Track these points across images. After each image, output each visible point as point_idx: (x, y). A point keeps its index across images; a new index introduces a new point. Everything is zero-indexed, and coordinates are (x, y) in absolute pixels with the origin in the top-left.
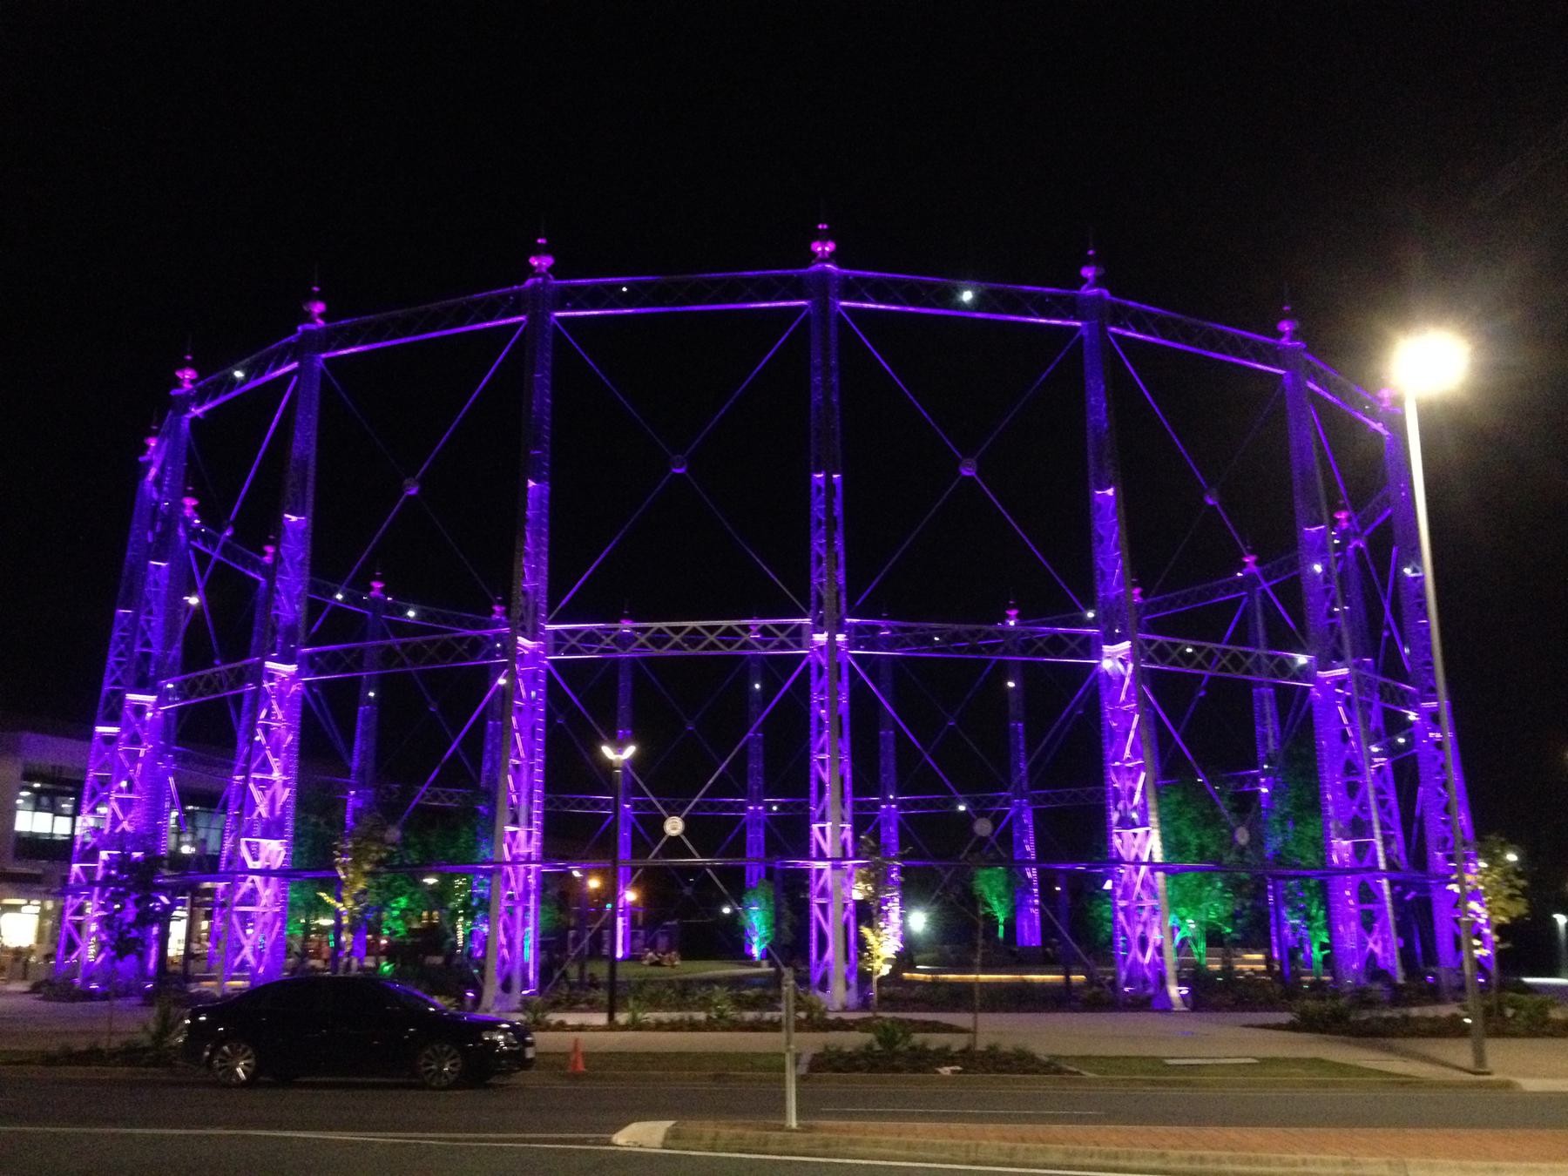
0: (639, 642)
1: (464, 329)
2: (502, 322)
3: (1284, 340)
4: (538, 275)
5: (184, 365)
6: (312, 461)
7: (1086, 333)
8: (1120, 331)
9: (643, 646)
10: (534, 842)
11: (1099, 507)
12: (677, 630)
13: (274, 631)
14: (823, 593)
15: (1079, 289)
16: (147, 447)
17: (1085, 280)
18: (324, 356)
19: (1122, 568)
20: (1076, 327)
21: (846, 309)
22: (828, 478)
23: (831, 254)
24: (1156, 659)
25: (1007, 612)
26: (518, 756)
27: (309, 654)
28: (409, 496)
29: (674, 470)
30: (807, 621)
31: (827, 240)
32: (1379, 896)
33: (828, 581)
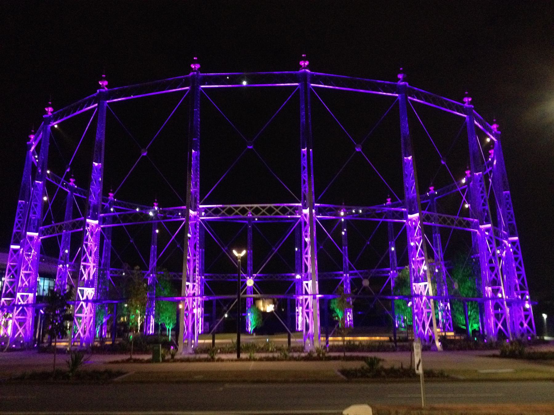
0: (222, 213)
1: (164, 92)
2: (180, 89)
3: (465, 104)
4: (195, 71)
5: (48, 106)
6: (103, 142)
7: (400, 99)
8: (412, 99)
9: (237, 214)
10: (196, 288)
11: (406, 164)
12: (237, 208)
13: (89, 209)
14: (306, 194)
15: (397, 82)
16: (30, 139)
17: (399, 79)
18: (108, 101)
19: (415, 186)
20: (397, 97)
21: (313, 87)
22: (308, 150)
23: (307, 66)
24: (426, 220)
25: (387, 199)
26: (189, 255)
27: (103, 217)
28: (143, 156)
29: (248, 147)
30: (300, 204)
31: (306, 61)
32: (503, 308)
33: (308, 189)
